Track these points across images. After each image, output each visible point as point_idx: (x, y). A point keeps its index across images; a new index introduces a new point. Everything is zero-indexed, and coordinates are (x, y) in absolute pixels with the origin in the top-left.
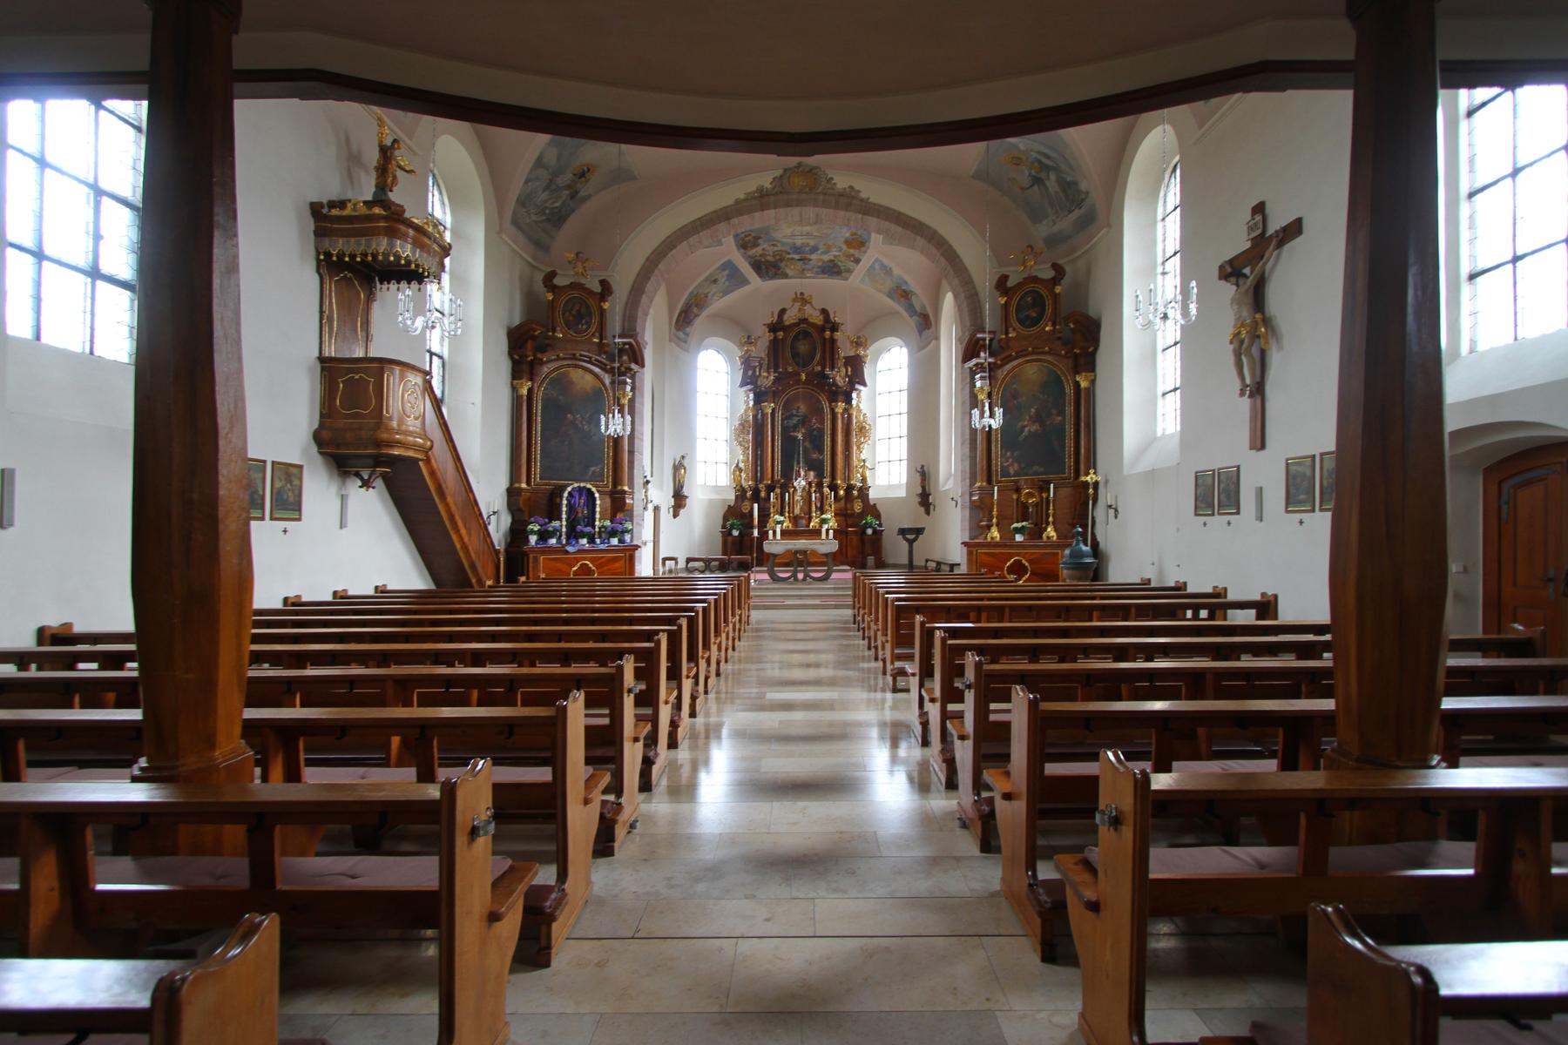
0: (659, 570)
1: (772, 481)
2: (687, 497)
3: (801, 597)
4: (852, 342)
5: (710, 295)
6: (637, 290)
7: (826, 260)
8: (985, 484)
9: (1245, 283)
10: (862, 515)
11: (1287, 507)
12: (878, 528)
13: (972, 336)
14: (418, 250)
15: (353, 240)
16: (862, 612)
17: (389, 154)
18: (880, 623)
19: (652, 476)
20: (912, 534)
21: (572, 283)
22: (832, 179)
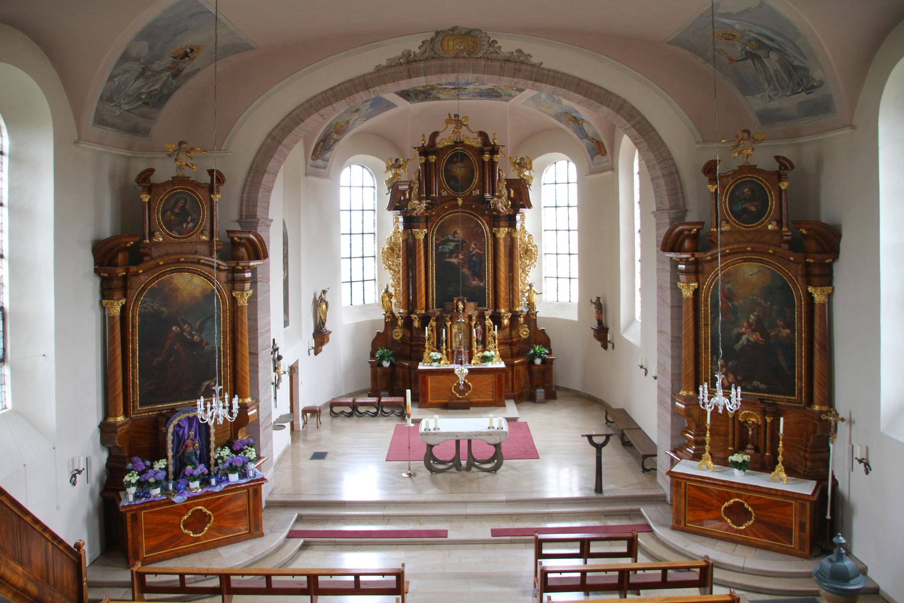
4: (515, 163)
5: (351, 122)
8: (691, 393)
22: (495, 42)
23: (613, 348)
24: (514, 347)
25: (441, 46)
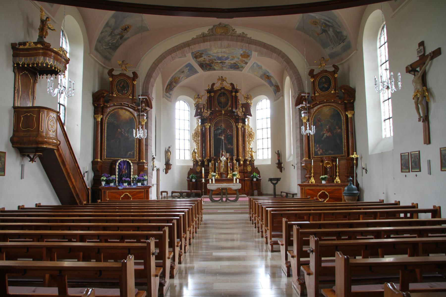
0: (159, 197)
1: (210, 158)
2: (172, 165)
3: (225, 209)
5: (181, 78)
6: (149, 76)
7: (232, 63)
8: (307, 159)
9: (418, 74)
10: (251, 172)
11: (441, 169)
12: (259, 178)
13: (299, 95)
14: (56, 61)
15: (28, 58)
16: (254, 216)
17: (44, 23)
18: (264, 221)
19: (156, 156)
20: (275, 181)
21: (120, 74)
22: (234, 29)
23: (284, 170)
24: (245, 174)
25: (215, 30)
